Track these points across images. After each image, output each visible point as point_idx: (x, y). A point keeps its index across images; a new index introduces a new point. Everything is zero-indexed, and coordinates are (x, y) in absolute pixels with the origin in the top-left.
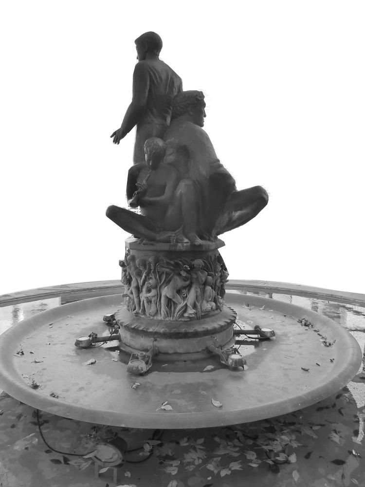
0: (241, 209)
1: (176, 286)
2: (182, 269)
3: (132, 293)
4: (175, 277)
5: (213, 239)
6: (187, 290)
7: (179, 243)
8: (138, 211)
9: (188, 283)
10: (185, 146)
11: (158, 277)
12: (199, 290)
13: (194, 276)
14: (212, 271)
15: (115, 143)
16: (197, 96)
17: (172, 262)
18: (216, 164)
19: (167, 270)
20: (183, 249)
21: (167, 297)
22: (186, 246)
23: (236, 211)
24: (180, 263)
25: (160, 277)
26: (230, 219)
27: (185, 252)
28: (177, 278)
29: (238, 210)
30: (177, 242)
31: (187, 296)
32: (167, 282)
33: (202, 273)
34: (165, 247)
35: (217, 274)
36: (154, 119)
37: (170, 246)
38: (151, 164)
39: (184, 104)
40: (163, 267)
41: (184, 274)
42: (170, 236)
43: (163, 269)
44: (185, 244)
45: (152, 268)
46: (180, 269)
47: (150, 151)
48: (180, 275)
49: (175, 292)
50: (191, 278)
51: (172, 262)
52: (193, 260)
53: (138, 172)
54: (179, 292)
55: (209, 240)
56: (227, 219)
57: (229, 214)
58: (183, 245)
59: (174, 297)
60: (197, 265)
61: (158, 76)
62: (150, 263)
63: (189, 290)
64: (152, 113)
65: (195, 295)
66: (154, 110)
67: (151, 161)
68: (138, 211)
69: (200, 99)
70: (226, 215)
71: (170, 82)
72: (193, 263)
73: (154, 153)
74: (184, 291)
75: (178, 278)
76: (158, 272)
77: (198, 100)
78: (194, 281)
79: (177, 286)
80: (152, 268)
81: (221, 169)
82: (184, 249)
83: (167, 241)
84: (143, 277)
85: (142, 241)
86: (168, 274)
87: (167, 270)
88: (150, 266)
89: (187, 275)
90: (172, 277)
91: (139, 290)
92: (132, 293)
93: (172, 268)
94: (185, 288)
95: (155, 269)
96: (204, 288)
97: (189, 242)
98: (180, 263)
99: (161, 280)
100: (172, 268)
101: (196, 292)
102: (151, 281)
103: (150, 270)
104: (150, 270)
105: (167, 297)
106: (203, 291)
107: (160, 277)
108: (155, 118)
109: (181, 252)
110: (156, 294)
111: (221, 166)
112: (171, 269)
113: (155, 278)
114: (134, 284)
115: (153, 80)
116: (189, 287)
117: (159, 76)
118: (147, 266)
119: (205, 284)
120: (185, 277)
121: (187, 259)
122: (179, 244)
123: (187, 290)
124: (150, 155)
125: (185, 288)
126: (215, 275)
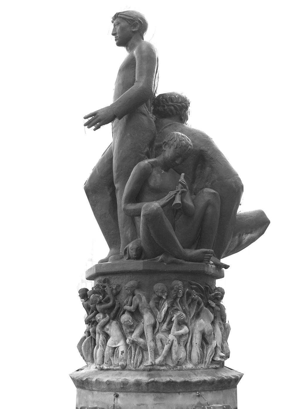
0: (251, 233)
23: (247, 233)
57: (240, 236)
70: (237, 237)
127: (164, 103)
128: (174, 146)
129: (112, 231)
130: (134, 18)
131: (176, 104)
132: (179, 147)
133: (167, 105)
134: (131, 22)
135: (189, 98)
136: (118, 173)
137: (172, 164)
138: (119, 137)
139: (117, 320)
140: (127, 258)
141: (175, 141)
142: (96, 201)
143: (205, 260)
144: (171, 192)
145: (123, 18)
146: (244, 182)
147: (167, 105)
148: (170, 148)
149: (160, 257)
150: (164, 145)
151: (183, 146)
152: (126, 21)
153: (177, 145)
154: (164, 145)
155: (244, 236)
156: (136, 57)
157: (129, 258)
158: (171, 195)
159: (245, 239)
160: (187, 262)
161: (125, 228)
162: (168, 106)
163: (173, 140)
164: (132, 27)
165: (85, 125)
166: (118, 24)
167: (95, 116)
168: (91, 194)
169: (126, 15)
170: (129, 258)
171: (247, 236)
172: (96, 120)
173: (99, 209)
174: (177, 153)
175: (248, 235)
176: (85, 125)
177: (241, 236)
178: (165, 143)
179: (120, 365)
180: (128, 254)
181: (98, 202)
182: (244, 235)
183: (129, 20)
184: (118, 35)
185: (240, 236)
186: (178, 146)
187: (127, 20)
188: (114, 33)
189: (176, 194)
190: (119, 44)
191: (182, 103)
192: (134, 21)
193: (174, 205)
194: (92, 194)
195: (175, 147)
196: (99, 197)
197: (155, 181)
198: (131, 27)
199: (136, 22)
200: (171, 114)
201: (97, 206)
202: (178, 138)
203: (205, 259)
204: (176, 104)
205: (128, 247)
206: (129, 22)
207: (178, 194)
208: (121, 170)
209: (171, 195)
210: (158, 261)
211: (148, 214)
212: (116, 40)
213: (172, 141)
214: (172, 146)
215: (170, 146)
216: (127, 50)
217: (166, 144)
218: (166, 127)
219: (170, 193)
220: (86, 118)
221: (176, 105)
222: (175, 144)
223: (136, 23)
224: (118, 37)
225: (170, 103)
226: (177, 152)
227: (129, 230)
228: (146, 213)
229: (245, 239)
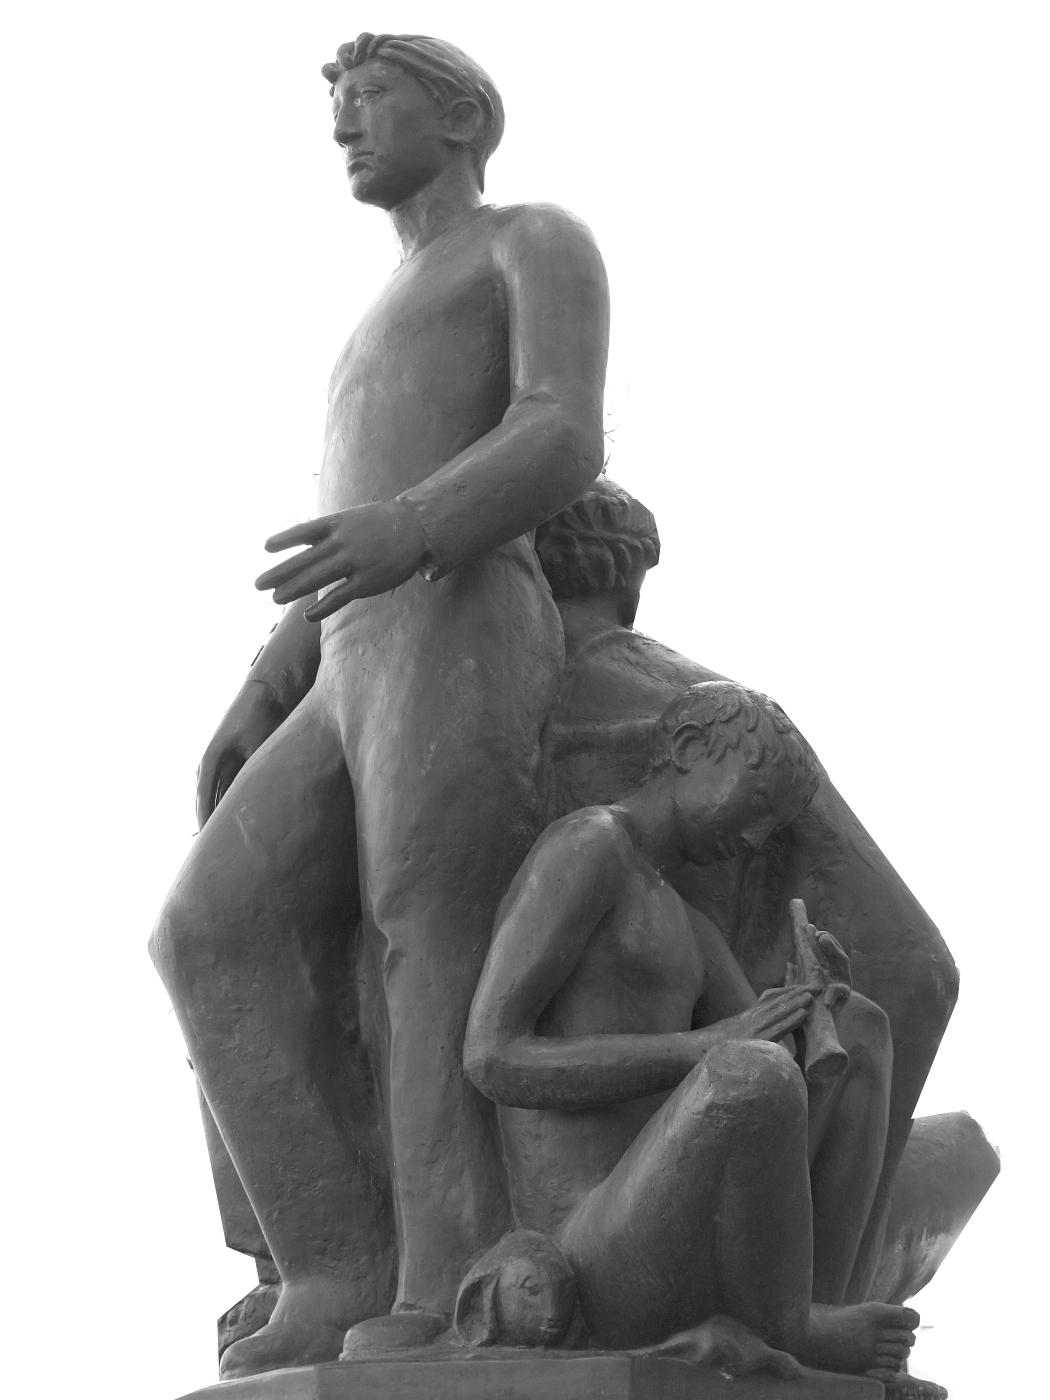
57: (908, 1245)
70: (899, 1247)
127: (569, 527)
128: (749, 753)
129: (321, 1183)
130: (459, 80)
132: (774, 761)
133: (584, 539)
134: (443, 94)
136: (409, 862)
137: (720, 844)
138: (410, 669)
140: (485, 1335)
141: (749, 731)
142: (235, 1007)
143: (879, 1360)
145: (408, 69)
146: (961, 962)
147: (584, 539)
148: (720, 760)
149: (704, 1339)
150: (680, 740)
151: (790, 760)
152: (422, 84)
153: (764, 749)
154: (680, 740)
155: (923, 1243)
157: (500, 1335)
158: (782, 1009)
160: (805, 1371)
161: (441, 1167)
162: (586, 540)
163: (740, 720)
164: (447, 122)
165: (263, 584)
166: (378, 90)
167: (324, 545)
168: (211, 960)
169: (423, 57)
170: (500, 1335)
172: (327, 565)
173: (251, 1049)
174: (758, 791)
175: (939, 1237)
176: (263, 584)
177: (913, 1245)
178: (685, 735)
180: (487, 1316)
181: (251, 1010)
182: (924, 1238)
183: (434, 81)
184: (368, 144)
185: (908, 1245)
186: (768, 759)
187: (428, 84)
188: (351, 130)
189: (809, 1005)
190: (366, 193)
191: (646, 536)
192: (461, 93)
193: (811, 1067)
194: (215, 964)
195: (754, 760)
197: (646, 923)
198: (442, 118)
199: (468, 99)
200: (594, 582)
201: (237, 1036)
202: (762, 714)
203: (880, 1355)
205: (497, 1276)
206: (437, 94)
207: (819, 1005)
208: (431, 851)
209: (776, 1012)
210: (698, 1358)
211: (751, 1103)
212: (354, 169)
213: (731, 725)
214: (729, 750)
215: (718, 754)
216: (405, 228)
217: (689, 740)
218: (593, 649)
219: (770, 997)
220: (274, 546)
221: (625, 542)
222: (753, 741)
223: (469, 103)
224: (375, 157)
225: (598, 531)
226: (761, 785)
227: (467, 1180)
228: (742, 1099)
229: (927, 1260)
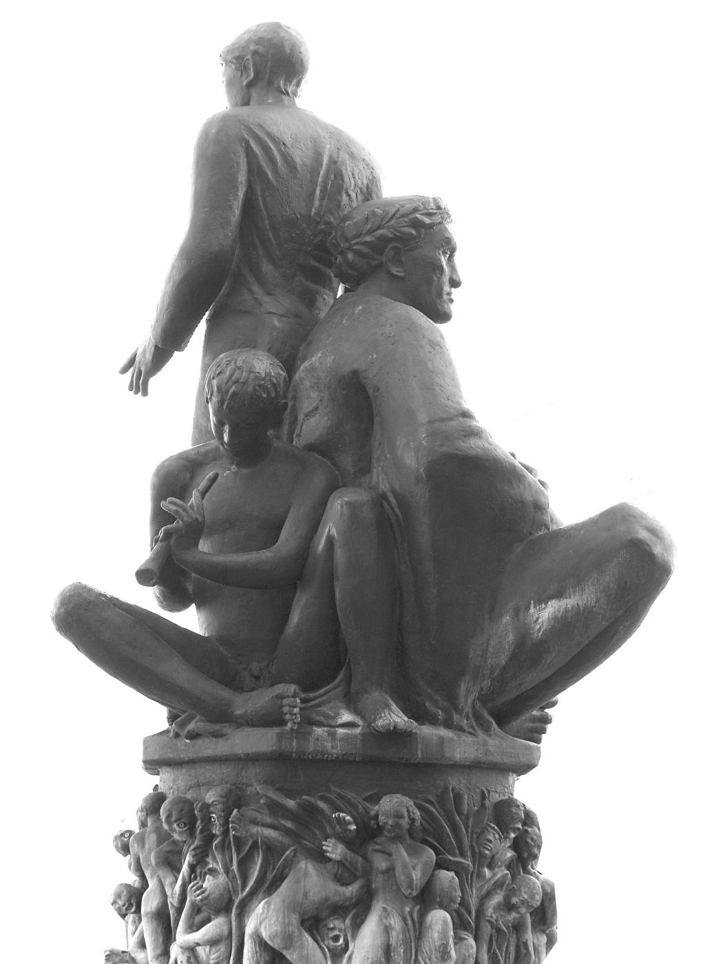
0: (559, 595)
1: (300, 897)
2: (328, 830)
3: (142, 945)
4: (302, 864)
5: (464, 723)
6: (348, 921)
7: (320, 724)
8: (191, 619)
9: (351, 890)
10: (355, 373)
11: (235, 867)
12: (395, 922)
13: (380, 863)
14: (462, 855)
15: (136, 393)
16: (416, 210)
17: (291, 803)
18: (454, 423)
19: (271, 833)
20: (334, 749)
21: (261, 943)
22: (345, 739)
23: (542, 600)
24: (321, 805)
25: (244, 864)
26: (523, 635)
27: (340, 762)
28: (306, 866)
29: (550, 598)
30: (309, 722)
31: (346, 948)
32: (267, 886)
33: (412, 852)
34: (261, 740)
35: (487, 872)
36: (266, 299)
37: (280, 737)
38: (226, 438)
39: (368, 239)
40: (254, 822)
41: (334, 850)
42: (281, 697)
43: (255, 829)
44: (341, 731)
45: (217, 830)
46: (323, 829)
47: (219, 388)
48: (320, 857)
49: (295, 919)
50: (368, 871)
51: (291, 803)
52: (374, 799)
53: (188, 476)
54: (313, 922)
55: (448, 724)
56: (511, 637)
57: (517, 613)
58: (332, 735)
59: (289, 940)
60: (387, 815)
61: (278, 158)
62: (206, 808)
63: (357, 925)
64: (261, 281)
65: (380, 941)
66: (266, 268)
67: (227, 428)
68: (191, 619)
69: (427, 220)
70: (506, 619)
71: (328, 172)
72: (375, 809)
73: (234, 394)
74: (337, 925)
75: (310, 867)
76: (239, 842)
77: (417, 224)
78: (378, 882)
79: (306, 895)
80: (217, 830)
81: (473, 442)
82: (337, 751)
83: (271, 719)
84: (185, 868)
85: (183, 725)
86: (271, 850)
87: (271, 833)
88: (207, 821)
89: (350, 855)
90: (288, 865)
91: (165, 925)
92: (142, 945)
93: (289, 824)
94: (338, 910)
95: (226, 833)
96: (423, 915)
97: (361, 723)
98: (321, 805)
99: (245, 878)
100: (289, 824)
101: (387, 930)
102: (209, 883)
103: (209, 838)
104: (209, 838)
105: (261, 943)
106: (418, 929)
107: (244, 864)
108: (270, 294)
109: (321, 763)
110: (226, 933)
111: (476, 433)
112: (287, 832)
113: (227, 871)
114: (149, 903)
115: (260, 167)
116: (358, 910)
117: (280, 151)
118: (199, 825)
119: (426, 898)
120: (340, 863)
121: (350, 795)
122: (319, 731)
123: (348, 921)
124: (221, 402)
125: (338, 910)
126: (480, 875)
131: (357, 240)
135: (51, 627)
139: (282, 718)
144: (496, 828)
155: (532, 610)
156: (263, 891)
159: (538, 619)
171: (544, 609)
177: (521, 614)
179: (287, 722)
182: (532, 605)
185: (517, 613)
196: (230, 234)
204: (357, 240)
221: (357, 244)
229: (540, 620)
